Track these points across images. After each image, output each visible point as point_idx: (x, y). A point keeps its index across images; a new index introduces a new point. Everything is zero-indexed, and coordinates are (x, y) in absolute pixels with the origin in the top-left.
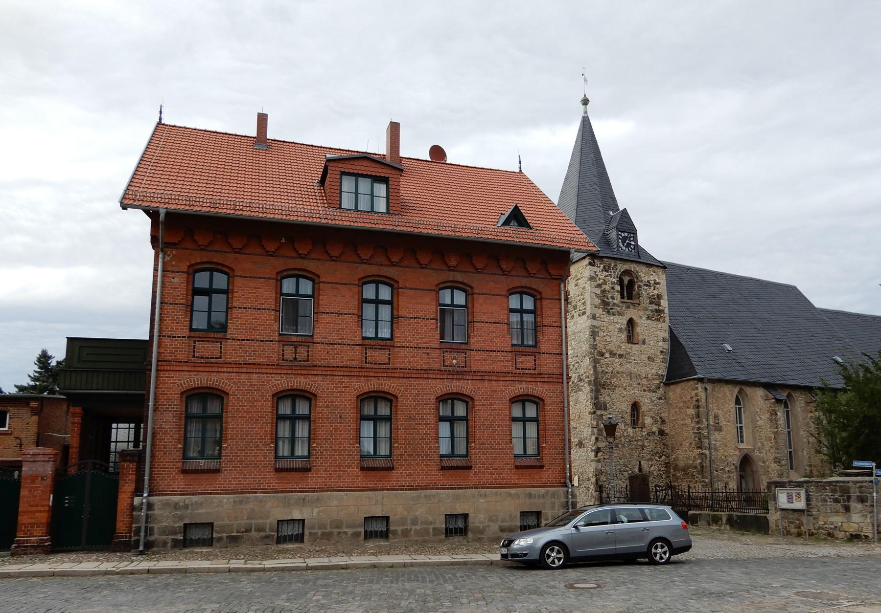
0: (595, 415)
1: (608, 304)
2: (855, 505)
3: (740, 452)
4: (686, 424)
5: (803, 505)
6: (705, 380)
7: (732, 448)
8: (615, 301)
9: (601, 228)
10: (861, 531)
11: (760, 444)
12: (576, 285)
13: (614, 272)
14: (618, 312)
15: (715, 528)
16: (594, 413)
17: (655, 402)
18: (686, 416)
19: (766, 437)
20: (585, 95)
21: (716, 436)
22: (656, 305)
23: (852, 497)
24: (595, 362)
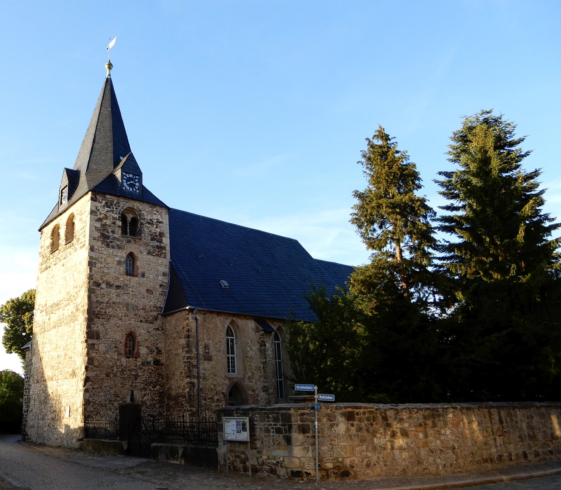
1: (108, 237)
2: (297, 437)
4: (178, 354)
8: (116, 236)
11: (250, 374)
13: (117, 208)
14: (118, 245)
17: (152, 333)
19: (256, 367)
20: (109, 61)
21: (205, 366)
22: (157, 241)
23: (293, 426)
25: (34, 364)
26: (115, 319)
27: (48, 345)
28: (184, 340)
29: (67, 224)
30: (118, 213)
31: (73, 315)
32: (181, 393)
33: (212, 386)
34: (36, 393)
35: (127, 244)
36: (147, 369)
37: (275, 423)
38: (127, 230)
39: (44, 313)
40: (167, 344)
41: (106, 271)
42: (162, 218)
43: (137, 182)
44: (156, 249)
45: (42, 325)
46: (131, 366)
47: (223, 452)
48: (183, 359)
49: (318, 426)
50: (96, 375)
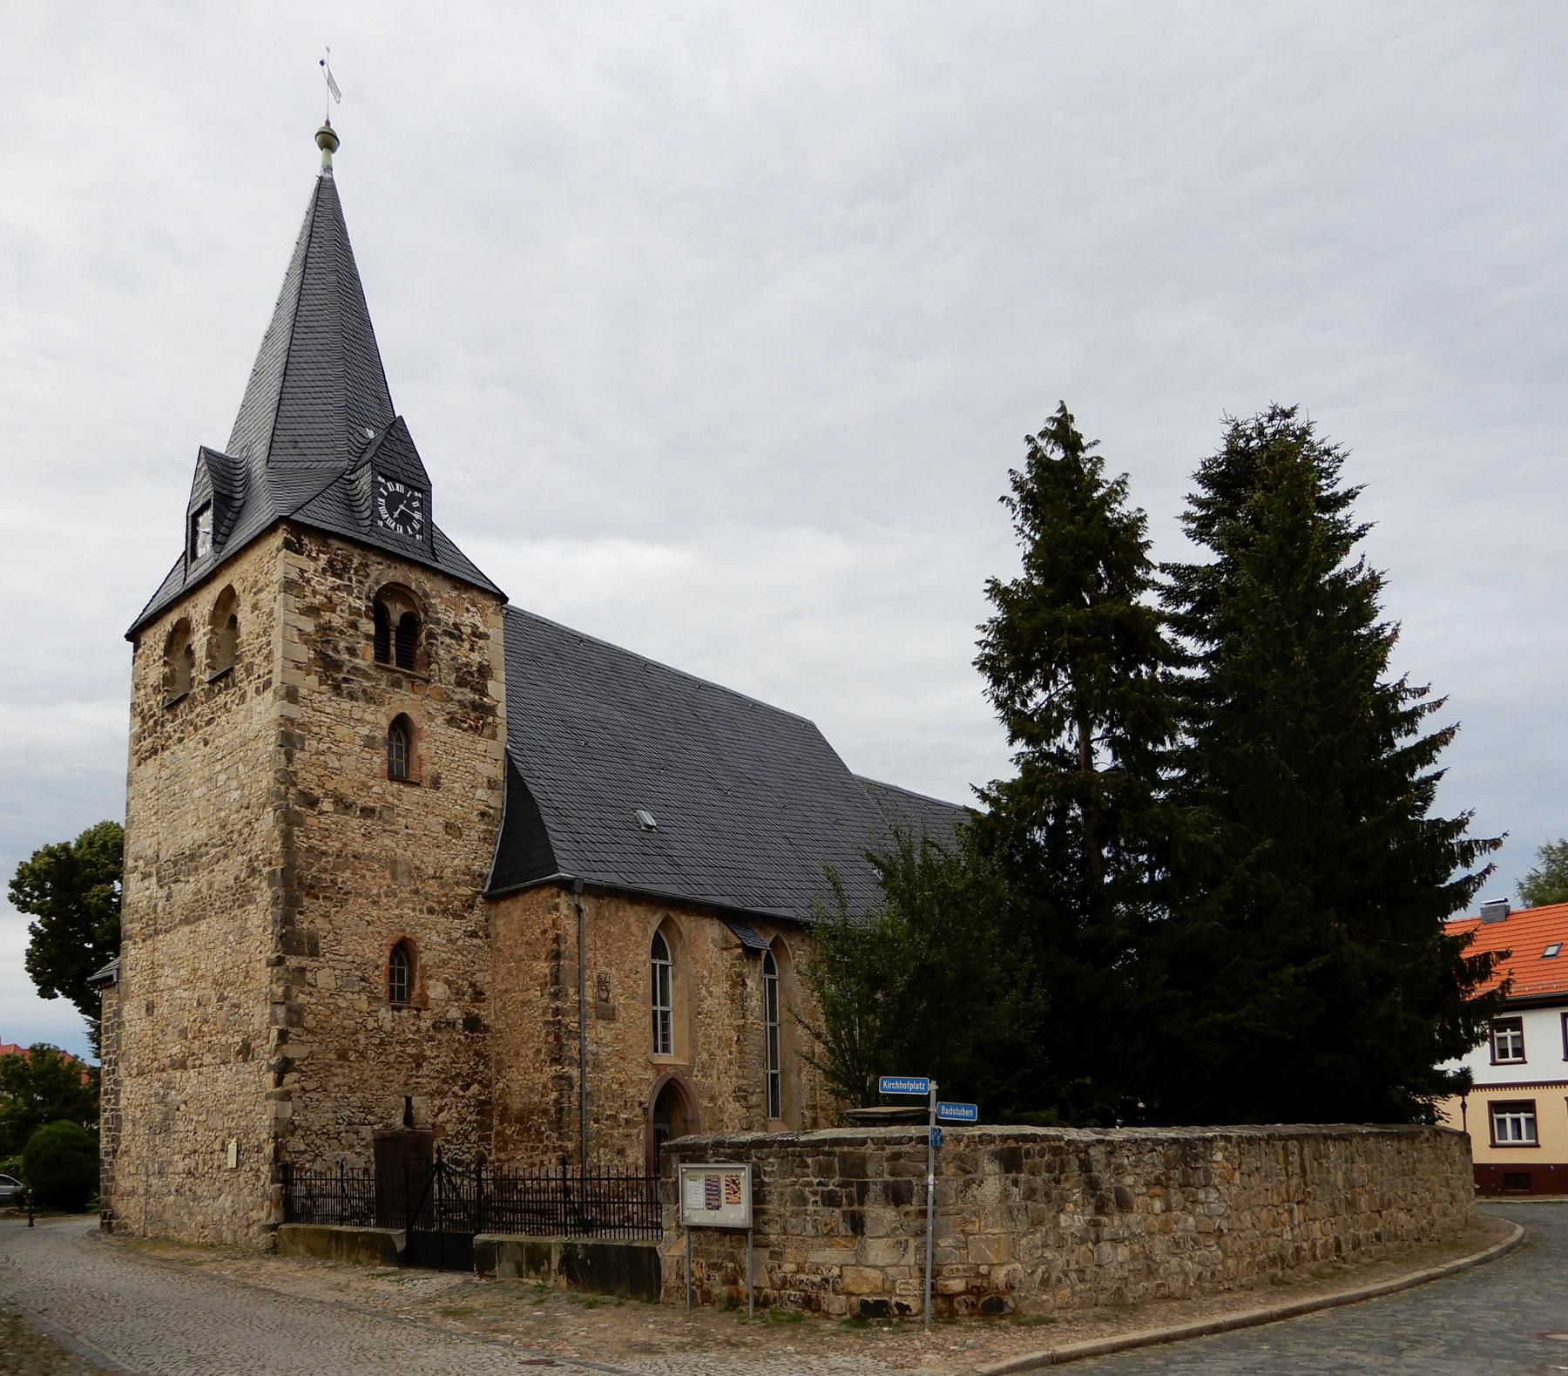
0: (281, 969)
1: (338, 666)
2: (880, 1214)
3: (658, 1072)
4: (530, 1000)
5: (743, 1215)
6: (578, 888)
7: (639, 1064)
9: (336, 464)
10: (890, 1292)
11: (705, 1056)
12: (255, 607)
13: (361, 582)
14: (364, 691)
15: (533, 1282)
16: (279, 962)
18: (532, 979)
19: (720, 1038)
20: (328, 123)
21: (600, 1032)
22: (474, 689)
23: (872, 1187)
24: (289, 820)
25: (127, 1025)
26: (360, 900)
27: (167, 971)
28: (544, 965)
29: (214, 618)
30: (364, 597)
31: (241, 887)
32: (536, 1103)
33: (615, 1087)
34: (138, 1103)
35: (391, 690)
36: (447, 1041)
37: (822, 1180)
38: (388, 651)
39: (154, 879)
40: (500, 976)
41: (333, 763)
42: (485, 622)
43: (417, 509)
44: (469, 710)
45: (148, 915)
46: (404, 1031)
47: (673, 1256)
48: (544, 1014)
49: (935, 1185)
50: (312, 1055)
